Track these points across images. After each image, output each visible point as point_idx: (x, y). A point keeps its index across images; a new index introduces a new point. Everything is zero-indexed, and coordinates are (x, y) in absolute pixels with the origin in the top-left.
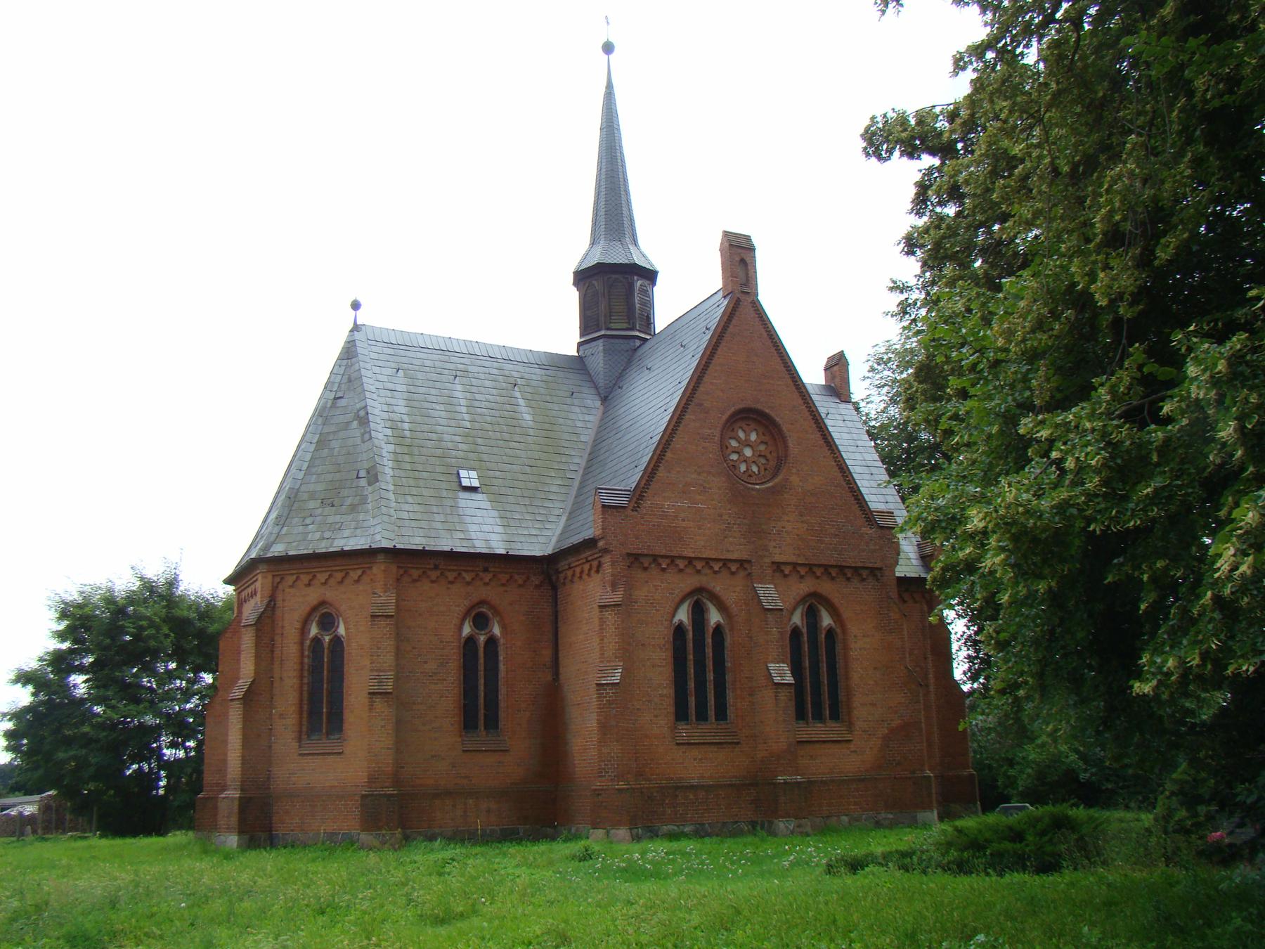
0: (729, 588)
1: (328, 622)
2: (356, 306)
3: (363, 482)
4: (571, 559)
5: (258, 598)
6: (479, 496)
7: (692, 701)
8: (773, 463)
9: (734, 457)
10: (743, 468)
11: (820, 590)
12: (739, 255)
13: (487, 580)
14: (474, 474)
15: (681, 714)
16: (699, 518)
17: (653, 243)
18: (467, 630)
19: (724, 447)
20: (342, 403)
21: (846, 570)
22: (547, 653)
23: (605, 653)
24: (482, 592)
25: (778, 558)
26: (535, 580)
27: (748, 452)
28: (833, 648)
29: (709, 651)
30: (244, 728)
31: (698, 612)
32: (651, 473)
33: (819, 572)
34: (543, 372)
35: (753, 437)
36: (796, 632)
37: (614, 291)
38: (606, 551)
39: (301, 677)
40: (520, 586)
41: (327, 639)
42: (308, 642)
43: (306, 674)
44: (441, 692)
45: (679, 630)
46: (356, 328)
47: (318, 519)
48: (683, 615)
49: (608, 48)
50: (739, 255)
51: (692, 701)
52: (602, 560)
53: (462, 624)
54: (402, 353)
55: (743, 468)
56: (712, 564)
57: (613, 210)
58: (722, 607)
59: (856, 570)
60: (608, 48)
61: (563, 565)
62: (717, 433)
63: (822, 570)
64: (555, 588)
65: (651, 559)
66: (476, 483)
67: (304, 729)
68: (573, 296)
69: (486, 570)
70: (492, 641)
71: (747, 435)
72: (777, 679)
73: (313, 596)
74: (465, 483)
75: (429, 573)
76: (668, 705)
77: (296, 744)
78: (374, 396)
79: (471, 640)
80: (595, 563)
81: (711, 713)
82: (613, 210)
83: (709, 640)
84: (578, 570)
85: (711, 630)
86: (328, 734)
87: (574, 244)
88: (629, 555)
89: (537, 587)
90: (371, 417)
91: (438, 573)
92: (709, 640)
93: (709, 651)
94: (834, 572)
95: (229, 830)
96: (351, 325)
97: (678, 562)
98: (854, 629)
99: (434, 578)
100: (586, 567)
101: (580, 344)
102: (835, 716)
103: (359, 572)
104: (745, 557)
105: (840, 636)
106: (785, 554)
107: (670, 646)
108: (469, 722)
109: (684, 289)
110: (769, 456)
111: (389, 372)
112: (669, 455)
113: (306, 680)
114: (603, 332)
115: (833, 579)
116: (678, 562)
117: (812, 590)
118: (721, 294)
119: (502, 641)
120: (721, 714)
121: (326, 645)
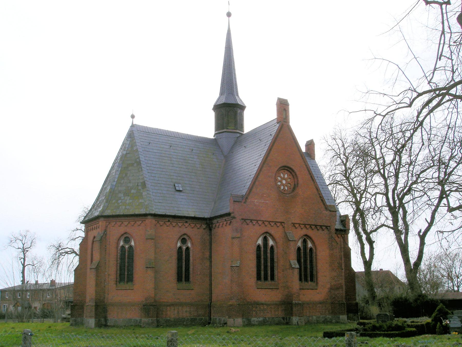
0: (277, 232)
1: (127, 240)
2: (133, 117)
3: (140, 188)
4: (218, 219)
5: (99, 230)
6: (182, 194)
7: (262, 273)
8: (293, 186)
9: (279, 183)
10: (282, 188)
11: (308, 234)
12: (283, 107)
13: (187, 226)
14: (180, 185)
15: (259, 278)
16: (266, 206)
17: (244, 94)
18: (179, 244)
19: (276, 180)
20: (128, 155)
21: (318, 227)
22: (207, 254)
23: (233, 256)
24: (185, 230)
25: (293, 222)
26: (204, 226)
27: (284, 182)
28: (312, 255)
29: (269, 255)
30: (96, 279)
31: (265, 240)
32: (251, 189)
33: (308, 227)
34: (202, 145)
35: (286, 176)
36: (299, 249)
37: (229, 112)
38: (234, 218)
39: (117, 260)
40: (198, 228)
41: (127, 246)
42: (119, 248)
43: (118, 259)
44: (170, 267)
45: (259, 246)
46: (133, 126)
47: (123, 201)
48: (260, 242)
49: (229, 15)
50: (283, 107)
51: (262, 273)
52: (232, 221)
53: (177, 242)
54: (151, 136)
55: (282, 188)
56: (271, 223)
57: (229, 81)
58: (274, 239)
59: (321, 226)
60: (229, 15)
61: (215, 221)
62: (274, 175)
63: (309, 226)
64: (210, 230)
65: (249, 221)
66: (181, 189)
67: (118, 280)
68: (212, 115)
69: (186, 222)
70: (188, 249)
71: (284, 176)
72: (293, 266)
73: (122, 230)
74: (177, 188)
75: (166, 223)
76: (254, 274)
77: (115, 286)
78: (142, 153)
79: (180, 248)
80: (229, 221)
81: (269, 278)
82: (229, 81)
83: (269, 251)
84: (221, 223)
85: (270, 248)
86: (127, 282)
87: (213, 94)
88: (242, 219)
89: (204, 229)
90: (141, 162)
91: (169, 223)
92: (269, 251)
93: (269, 255)
94: (313, 227)
95: (91, 317)
96: (131, 125)
97: (259, 222)
98: (319, 249)
99: (168, 225)
100: (225, 223)
101: (215, 134)
102: (312, 280)
103: (141, 222)
104: (282, 221)
105: (314, 251)
106: (297, 221)
107: (255, 253)
108: (179, 279)
109: (257, 116)
110: (291, 184)
111: (147, 144)
112: (257, 183)
113: (118, 262)
114: (225, 130)
115: (313, 229)
116: (259, 222)
117: (305, 234)
118: (276, 121)
119: (191, 249)
120: (272, 278)
121: (127, 249)
